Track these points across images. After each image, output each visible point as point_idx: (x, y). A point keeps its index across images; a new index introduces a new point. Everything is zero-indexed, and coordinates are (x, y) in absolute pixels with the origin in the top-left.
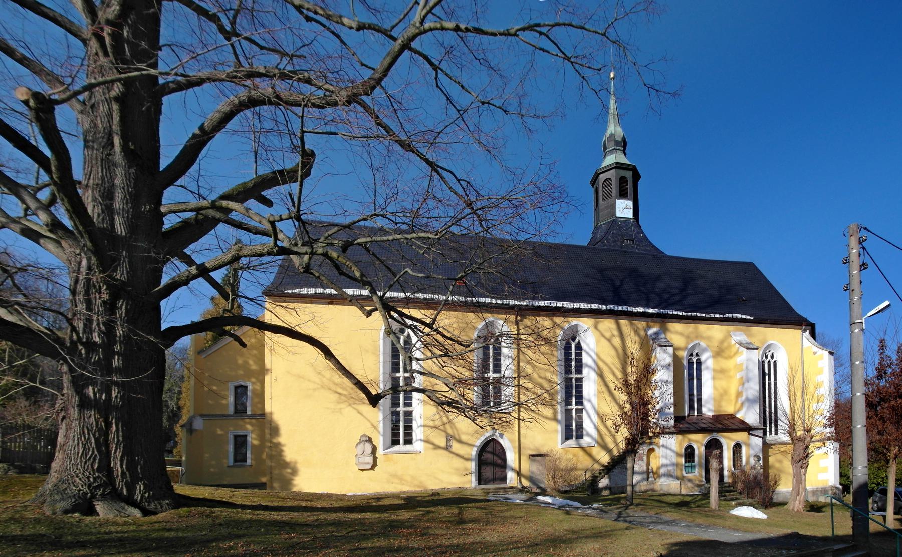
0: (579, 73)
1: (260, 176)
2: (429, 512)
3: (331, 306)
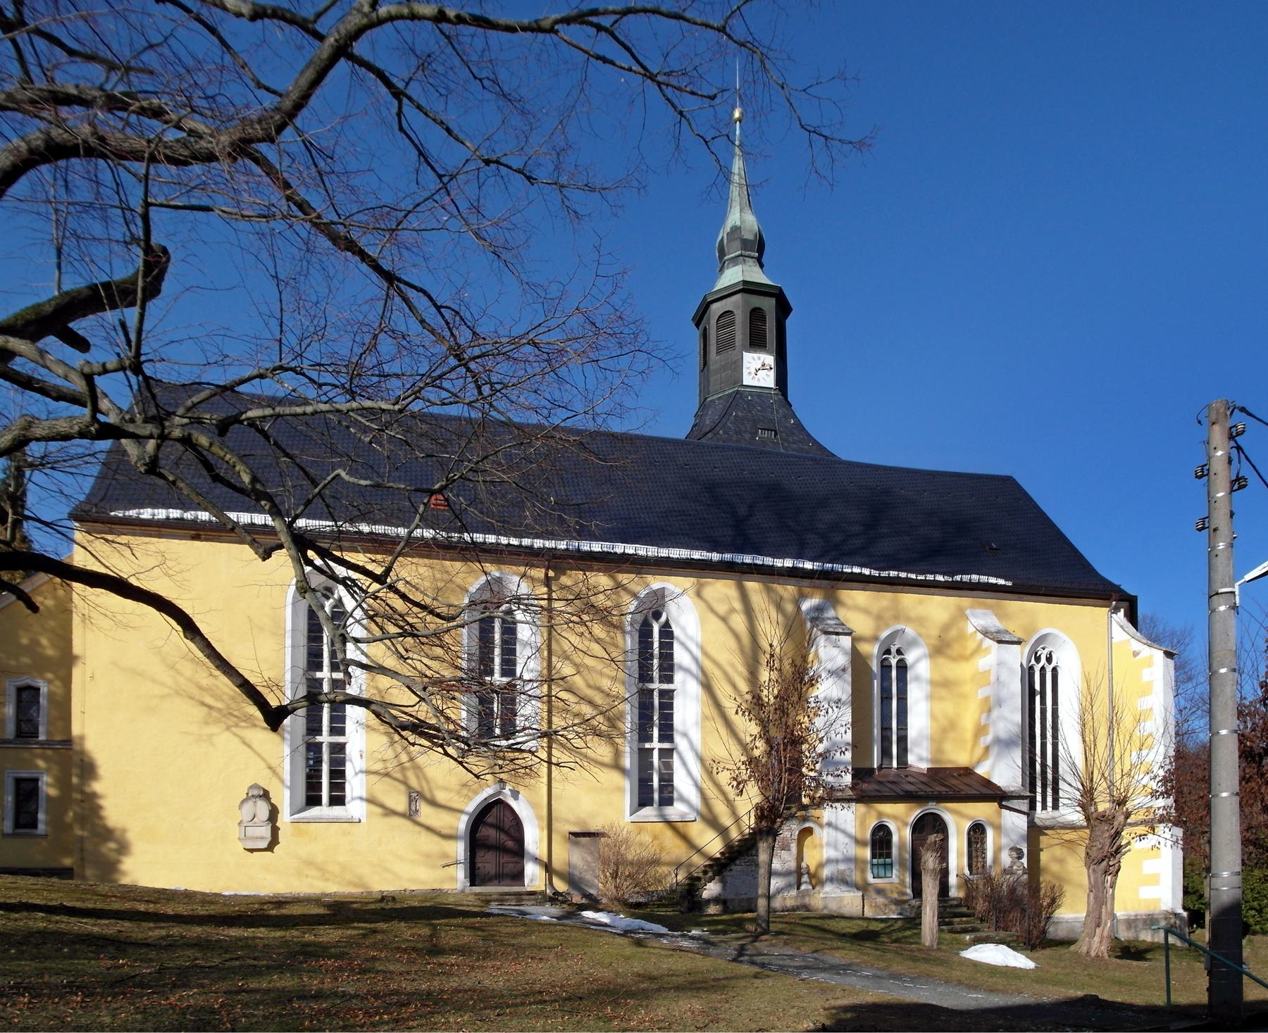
0: (673, 105)
1: (67, 293)
2: (375, 931)
3: (197, 543)
